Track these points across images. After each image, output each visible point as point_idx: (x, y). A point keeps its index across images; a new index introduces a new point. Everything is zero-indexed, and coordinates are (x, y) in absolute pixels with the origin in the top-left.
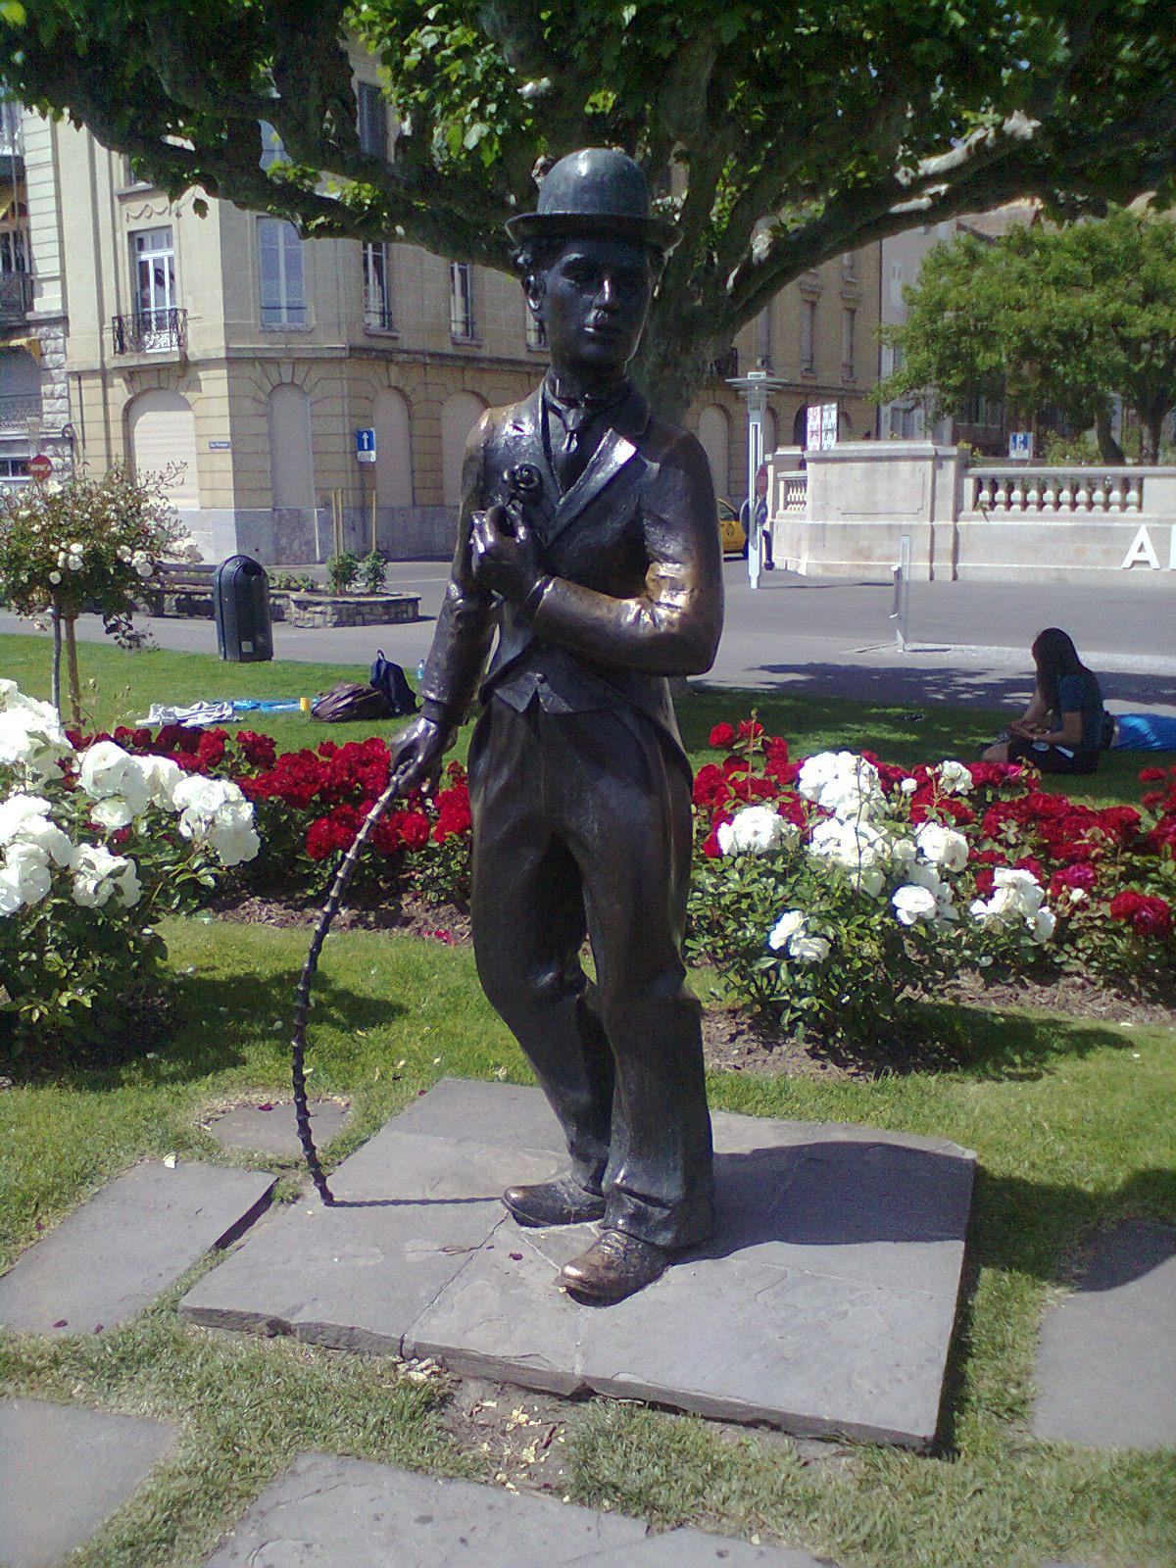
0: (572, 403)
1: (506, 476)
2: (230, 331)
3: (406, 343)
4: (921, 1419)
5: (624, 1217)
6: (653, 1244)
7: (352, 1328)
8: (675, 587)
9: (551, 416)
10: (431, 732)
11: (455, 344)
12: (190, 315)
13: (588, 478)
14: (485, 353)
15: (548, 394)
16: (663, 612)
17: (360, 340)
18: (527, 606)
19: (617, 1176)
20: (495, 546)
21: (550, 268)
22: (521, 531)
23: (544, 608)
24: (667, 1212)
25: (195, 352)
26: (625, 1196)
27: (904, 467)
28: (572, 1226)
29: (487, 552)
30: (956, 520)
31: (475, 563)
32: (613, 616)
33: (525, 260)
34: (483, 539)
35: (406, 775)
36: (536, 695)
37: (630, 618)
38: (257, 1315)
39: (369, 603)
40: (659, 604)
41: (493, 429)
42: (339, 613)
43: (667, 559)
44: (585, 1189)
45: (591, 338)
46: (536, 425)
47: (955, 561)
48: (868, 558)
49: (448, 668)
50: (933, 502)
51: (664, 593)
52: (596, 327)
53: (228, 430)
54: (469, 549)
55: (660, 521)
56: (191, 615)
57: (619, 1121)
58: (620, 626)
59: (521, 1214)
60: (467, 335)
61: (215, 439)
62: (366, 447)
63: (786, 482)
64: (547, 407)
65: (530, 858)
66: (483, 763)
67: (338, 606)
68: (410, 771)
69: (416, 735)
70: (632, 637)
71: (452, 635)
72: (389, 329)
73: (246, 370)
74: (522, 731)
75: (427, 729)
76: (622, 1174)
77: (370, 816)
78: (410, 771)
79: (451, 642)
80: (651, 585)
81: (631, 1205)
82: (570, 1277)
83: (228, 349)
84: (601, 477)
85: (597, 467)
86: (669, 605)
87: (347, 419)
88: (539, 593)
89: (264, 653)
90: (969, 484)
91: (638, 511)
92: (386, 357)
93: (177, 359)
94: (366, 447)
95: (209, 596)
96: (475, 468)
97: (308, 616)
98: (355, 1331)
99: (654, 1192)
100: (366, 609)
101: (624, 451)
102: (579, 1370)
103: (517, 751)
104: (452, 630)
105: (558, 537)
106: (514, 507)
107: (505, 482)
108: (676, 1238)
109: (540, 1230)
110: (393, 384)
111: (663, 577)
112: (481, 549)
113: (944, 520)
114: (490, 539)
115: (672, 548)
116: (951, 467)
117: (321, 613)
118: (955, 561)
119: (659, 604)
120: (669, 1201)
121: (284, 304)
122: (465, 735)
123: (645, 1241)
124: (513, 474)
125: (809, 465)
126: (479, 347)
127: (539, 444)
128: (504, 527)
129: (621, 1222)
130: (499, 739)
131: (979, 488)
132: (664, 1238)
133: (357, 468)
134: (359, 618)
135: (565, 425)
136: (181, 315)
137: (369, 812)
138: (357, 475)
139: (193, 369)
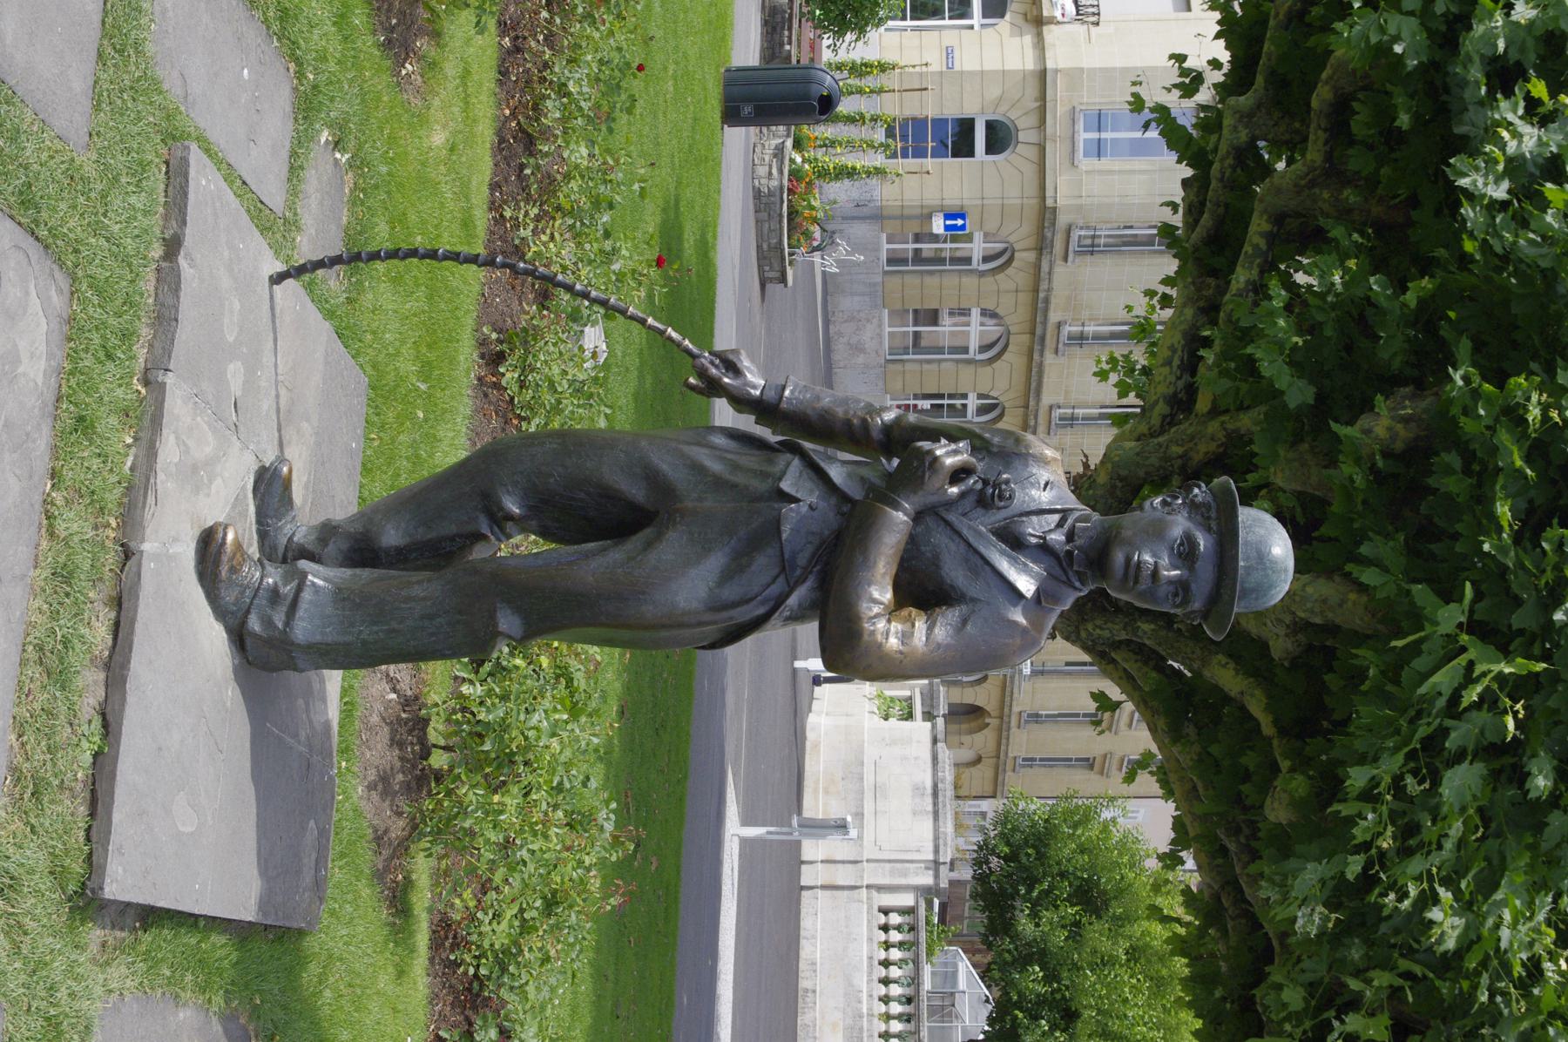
0: (1070, 537)
1: (1005, 476)
2: (1075, 75)
3: (1060, 270)
4: (120, 884)
5: (276, 583)
6: (248, 612)
7: (177, 320)
8: (905, 637)
9: (1056, 517)
10: (752, 391)
11: (1059, 325)
12: (1093, 29)
13: (1003, 553)
14: (1049, 358)
15: (1077, 514)
16: (881, 625)
17: (1063, 220)
18: (886, 492)
19: (314, 576)
20: (942, 464)
21: (1190, 518)
22: (954, 490)
23: (886, 512)
24: (280, 625)
25: (1050, 33)
26: (294, 584)
27: (927, 825)
28: (254, 528)
29: (936, 459)
30: (868, 887)
31: (925, 445)
32: (879, 577)
33: (1196, 496)
34: (948, 454)
35: (709, 366)
36: (797, 500)
37: (876, 595)
38: (184, 223)
39: (781, 229)
40: (889, 621)
41: (1043, 461)
42: (771, 194)
43: (930, 629)
44: (290, 539)
45: (1128, 560)
46: (1051, 503)
47: (824, 887)
48: (826, 792)
49: (814, 409)
50: (889, 861)
51: (900, 627)
52: (1139, 562)
53: (967, 67)
54: (934, 435)
55: (964, 622)
56: (765, 23)
57: (366, 574)
58: (869, 585)
59: (268, 476)
60: (1069, 339)
61: (957, 54)
62: (948, 222)
63: (911, 698)
64: (1065, 513)
65: (636, 492)
66: (719, 440)
67: (778, 193)
68: (714, 371)
69: (749, 375)
70: (859, 597)
71: (846, 412)
72: (1075, 252)
73: (1032, 91)
74: (760, 486)
75: (754, 387)
76: (316, 580)
77: (670, 330)
78: (714, 371)
79: (840, 412)
80: (905, 612)
81: (287, 590)
82: (225, 534)
83: (1056, 71)
84: (1005, 566)
85: (1014, 561)
86: (888, 633)
87: (980, 202)
88: (896, 507)
89: (732, 115)
90: (907, 900)
91: (974, 600)
92: (1042, 246)
93: (1045, 13)
94: (948, 222)
95: (1506, 1012)
96: (1010, 443)
97: (767, 158)
98: (174, 323)
99: (300, 613)
100: (774, 225)
101: (1026, 585)
102: (146, 547)
103: (740, 479)
104: (852, 412)
105: (948, 524)
106: (975, 482)
107: (999, 474)
108: (255, 635)
109: (250, 495)
110: (1016, 254)
111: (913, 625)
112: (938, 453)
113: (872, 875)
114: (949, 461)
115: (941, 633)
116: (927, 879)
117: (770, 173)
118: (824, 887)
119: (889, 621)
120: (291, 629)
121: (1104, 135)
122: (747, 423)
123: (251, 603)
124: (1007, 482)
125: (929, 725)
126: (1056, 351)
127: (1033, 507)
128: (959, 474)
129: (270, 581)
130: (751, 459)
131: (903, 911)
132: (254, 624)
133: (925, 211)
134: (764, 215)
135: (1050, 531)
136: (1094, 19)
137: (674, 329)
138: (918, 211)
139: (1034, 30)
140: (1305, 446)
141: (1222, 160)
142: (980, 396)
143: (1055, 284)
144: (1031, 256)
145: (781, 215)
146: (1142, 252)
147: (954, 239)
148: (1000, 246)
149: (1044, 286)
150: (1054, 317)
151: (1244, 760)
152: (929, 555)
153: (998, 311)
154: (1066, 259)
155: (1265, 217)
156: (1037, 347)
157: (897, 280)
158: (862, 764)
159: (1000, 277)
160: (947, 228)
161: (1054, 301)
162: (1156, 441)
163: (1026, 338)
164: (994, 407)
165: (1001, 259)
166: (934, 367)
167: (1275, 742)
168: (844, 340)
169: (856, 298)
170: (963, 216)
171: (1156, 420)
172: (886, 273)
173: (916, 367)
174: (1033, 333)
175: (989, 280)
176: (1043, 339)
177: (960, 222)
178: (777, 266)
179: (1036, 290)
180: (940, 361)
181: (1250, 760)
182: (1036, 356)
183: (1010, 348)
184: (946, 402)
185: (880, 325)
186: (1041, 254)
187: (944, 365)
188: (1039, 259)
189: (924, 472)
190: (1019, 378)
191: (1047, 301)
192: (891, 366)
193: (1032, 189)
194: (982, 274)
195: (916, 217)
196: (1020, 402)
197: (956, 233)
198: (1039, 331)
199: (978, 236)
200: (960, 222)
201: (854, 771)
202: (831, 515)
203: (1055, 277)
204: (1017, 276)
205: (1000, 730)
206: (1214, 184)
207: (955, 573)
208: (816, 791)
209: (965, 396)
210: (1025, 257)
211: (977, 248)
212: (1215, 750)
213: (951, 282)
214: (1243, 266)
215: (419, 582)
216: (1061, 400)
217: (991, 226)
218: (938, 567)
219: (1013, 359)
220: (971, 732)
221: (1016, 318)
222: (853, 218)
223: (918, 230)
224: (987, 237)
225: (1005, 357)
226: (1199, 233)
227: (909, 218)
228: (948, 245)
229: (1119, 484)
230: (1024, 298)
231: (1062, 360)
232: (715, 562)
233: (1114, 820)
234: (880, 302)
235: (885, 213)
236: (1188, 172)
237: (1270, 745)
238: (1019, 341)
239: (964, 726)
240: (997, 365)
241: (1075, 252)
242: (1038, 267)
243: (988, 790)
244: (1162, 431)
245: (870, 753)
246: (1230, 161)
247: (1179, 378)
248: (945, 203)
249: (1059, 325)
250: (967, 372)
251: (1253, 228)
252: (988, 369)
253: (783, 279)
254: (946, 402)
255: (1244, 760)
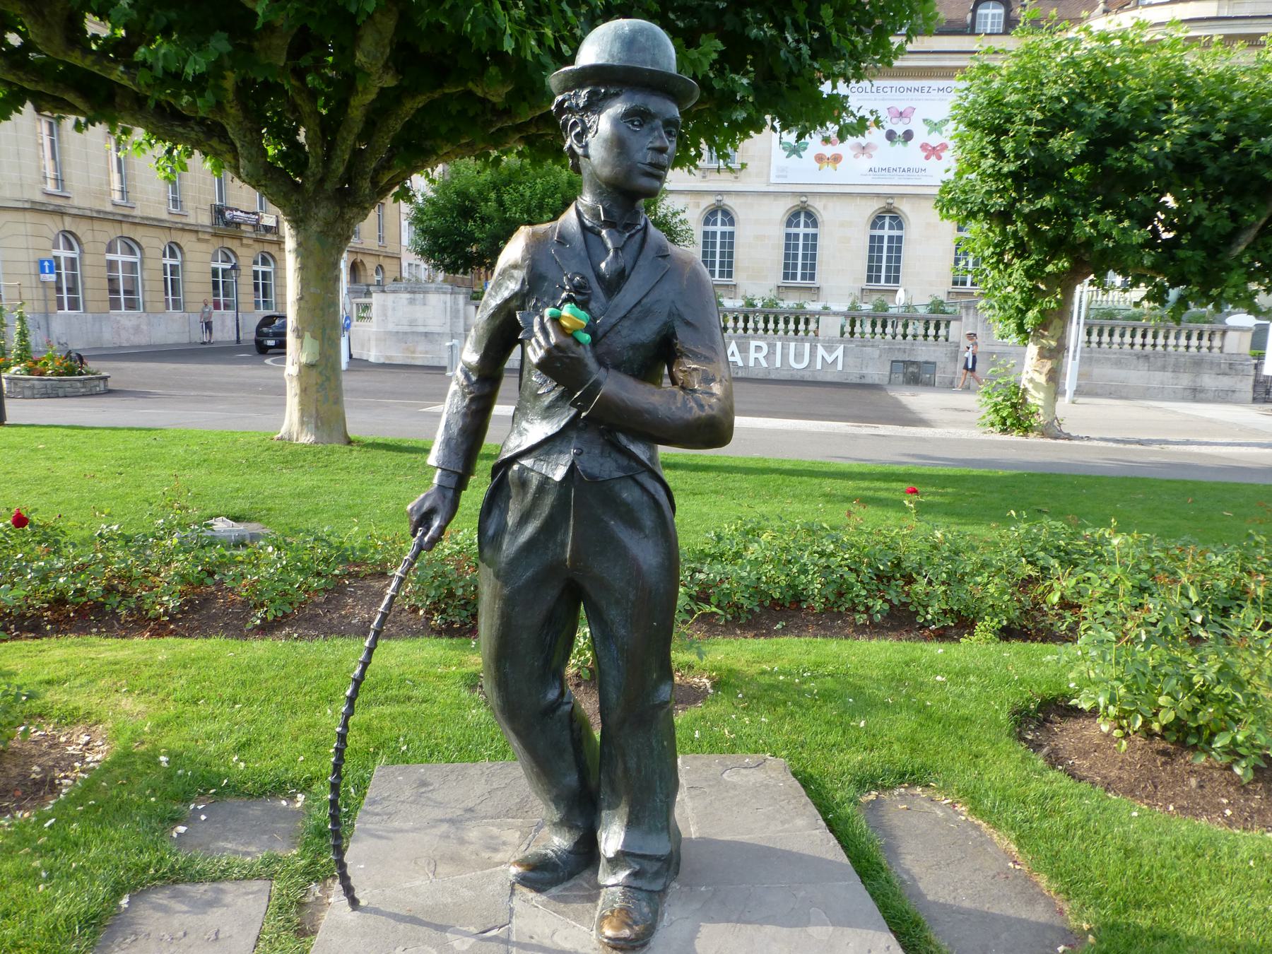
62: (47, 271)
92: (60, 213)
94: (47, 271)
100: (67, 384)
134: (61, 392)
140: (256, 45)
141: (21, 79)
142: (164, 256)
143: (86, 205)
144: (67, 220)
145: (60, 380)
146: (60, 148)
147: (58, 267)
148: (61, 238)
149: (88, 213)
150: (109, 208)
151: (454, 112)
152: (631, 353)
153: (107, 242)
154: (68, 198)
155: (70, 53)
156: (130, 220)
157: (89, 304)
158: (397, 332)
159: (83, 240)
160: (51, 272)
161: (98, 207)
162: (239, 149)
163: (124, 226)
164: (171, 248)
165: (69, 238)
166: (147, 283)
167: (447, 91)
168: (132, 337)
169: (104, 329)
170: (42, 262)
171: (223, 148)
172: (85, 311)
173: (147, 294)
174: (121, 222)
175: (86, 247)
176: (124, 216)
177: (46, 264)
178: (96, 382)
179: (91, 218)
180: (143, 280)
181: (454, 108)
182: (137, 221)
183: (74, 230)
184: (169, 277)
185: (121, 316)
186: (65, 213)
187: (145, 277)
188: (70, 215)
189: (569, 357)
190: (151, 232)
191: (99, 212)
192: (148, 309)
193: (19, 216)
194: (82, 251)
195: (45, 292)
196: (117, 225)
197: (55, 265)
198: (120, 218)
199: (55, 253)
200: (46, 264)
201: (400, 337)
202: (586, 436)
203: (82, 205)
204: (81, 229)
205: (364, 253)
206: (40, 88)
207: (647, 332)
208: (413, 358)
209: (165, 265)
210: (69, 224)
211: (63, 253)
212: (443, 129)
213: (88, 271)
214: (110, 74)
215: (625, 763)
216: (164, 207)
217: (49, 244)
218: (643, 345)
219: (138, 234)
220: (365, 269)
221: (112, 232)
222: (48, 330)
223: (54, 290)
224: (56, 246)
225: (137, 239)
226: (78, 103)
227: (45, 296)
228: (63, 272)
229: (269, 176)
230: (97, 225)
231: (138, 205)
232: (625, 536)
233: (423, 195)
234: (105, 315)
235: (43, 311)
236: (28, 108)
237: (447, 94)
238: (127, 231)
239: (362, 273)
240: (144, 246)
241: (63, 191)
242: (75, 216)
243: (395, 261)
244: (233, 144)
245: (391, 327)
246: (21, 74)
247: (193, 129)
248: (33, 272)
249: (114, 205)
250: (149, 263)
251: (79, 63)
252: (146, 250)
253: (105, 378)
254: (169, 277)
255: (454, 112)
